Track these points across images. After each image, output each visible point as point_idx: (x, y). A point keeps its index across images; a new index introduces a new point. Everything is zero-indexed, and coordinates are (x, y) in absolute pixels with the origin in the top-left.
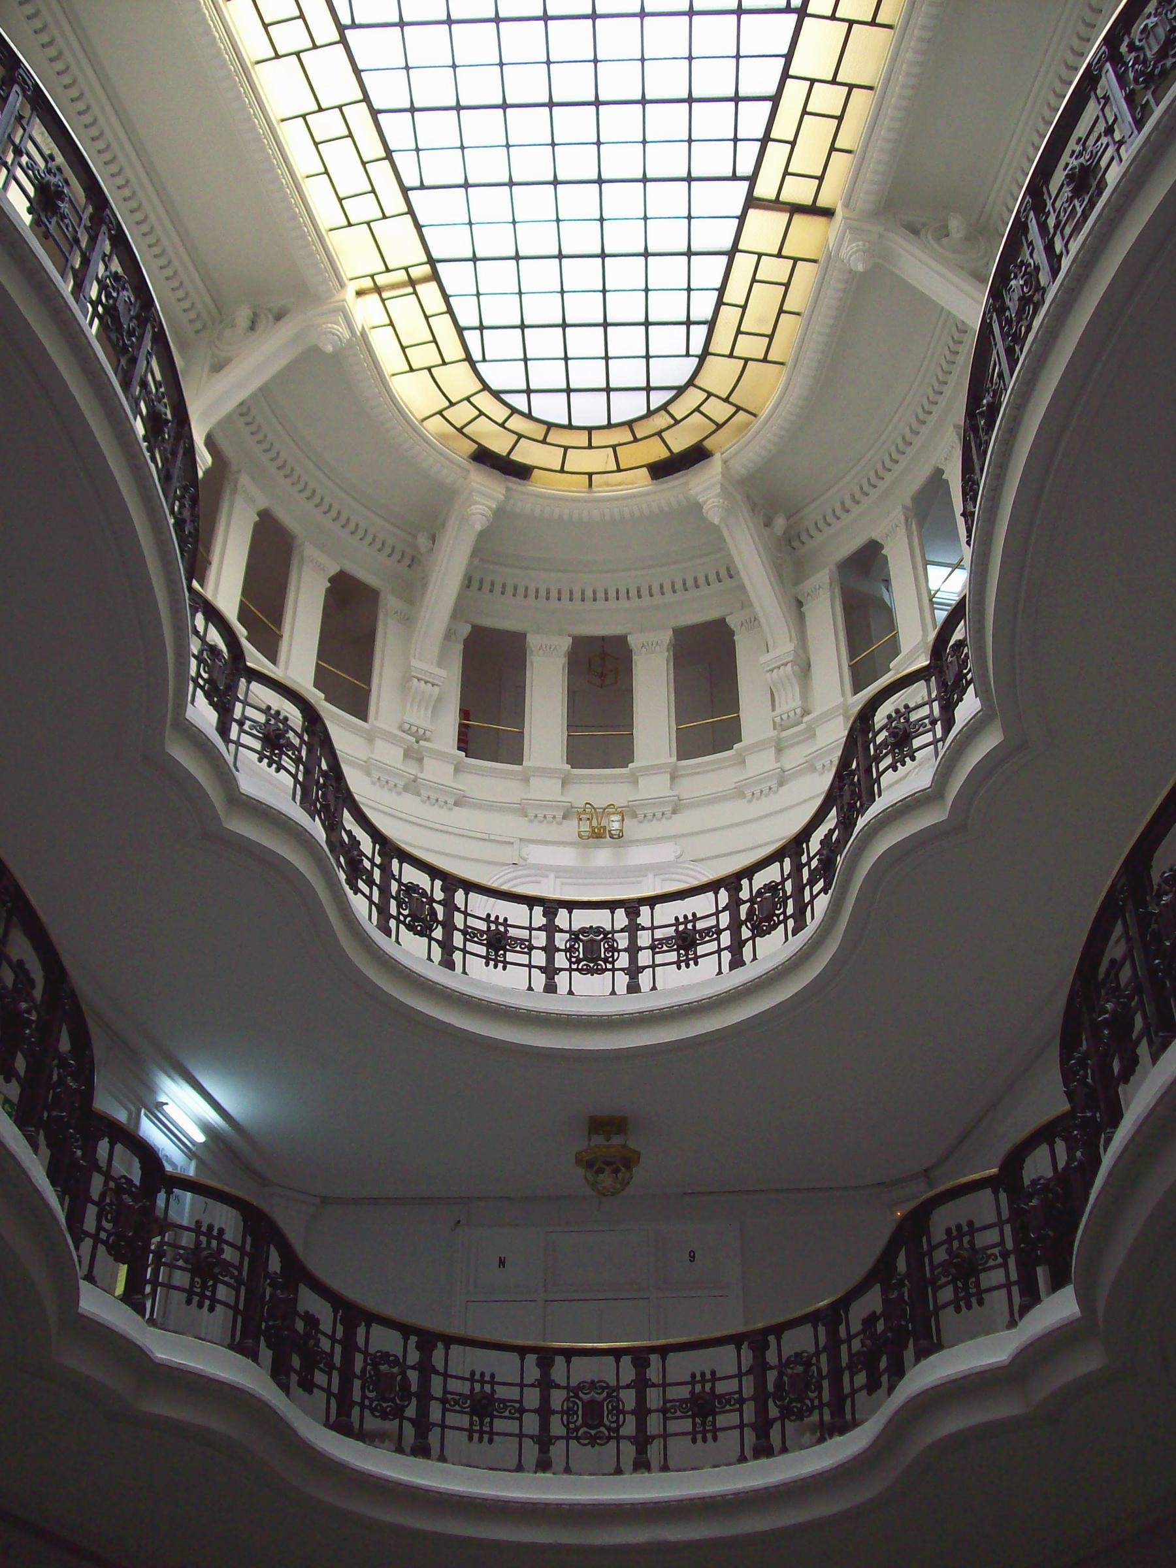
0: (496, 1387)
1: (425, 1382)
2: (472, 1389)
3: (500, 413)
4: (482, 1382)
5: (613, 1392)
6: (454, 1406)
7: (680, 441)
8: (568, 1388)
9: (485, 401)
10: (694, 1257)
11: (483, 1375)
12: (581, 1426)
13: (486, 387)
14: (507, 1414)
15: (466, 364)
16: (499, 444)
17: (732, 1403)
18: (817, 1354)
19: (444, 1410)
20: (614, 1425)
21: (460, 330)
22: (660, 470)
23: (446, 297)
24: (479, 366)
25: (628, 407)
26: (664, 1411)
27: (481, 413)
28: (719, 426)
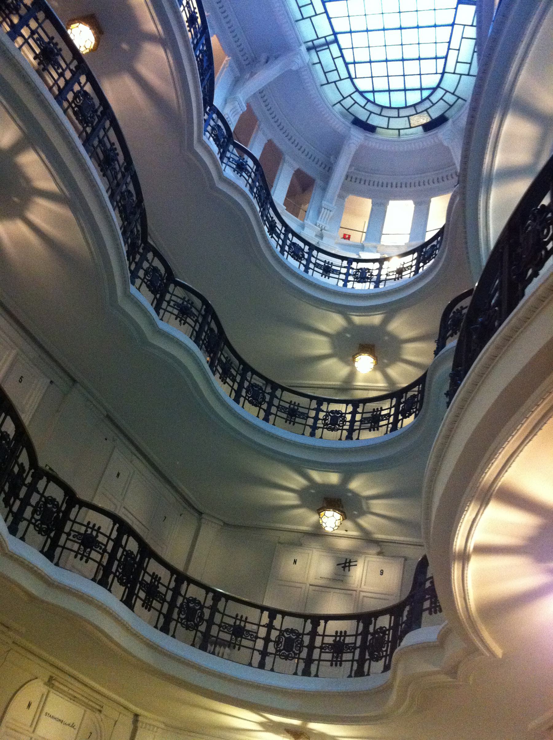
0: (247, 624)
1: (212, 616)
2: (235, 623)
3: (362, 102)
4: (241, 620)
5: (299, 635)
6: (224, 629)
7: (435, 113)
8: (280, 630)
9: (356, 96)
10: (382, 573)
11: (242, 617)
12: (283, 650)
13: (357, 90)
14: (249, 638)
15: (349, 80)
16: (363, 115)
17: (351, 648)
18: (389, 630)
19: (219, 631)
20: (298, 652)
21: (346, 64)
22: (427, 127)
23: (341, 50)
24: (355, 80)
25: (414, 98)
26: (321, 648)
27: (356, 102)
28: (451, 106)
